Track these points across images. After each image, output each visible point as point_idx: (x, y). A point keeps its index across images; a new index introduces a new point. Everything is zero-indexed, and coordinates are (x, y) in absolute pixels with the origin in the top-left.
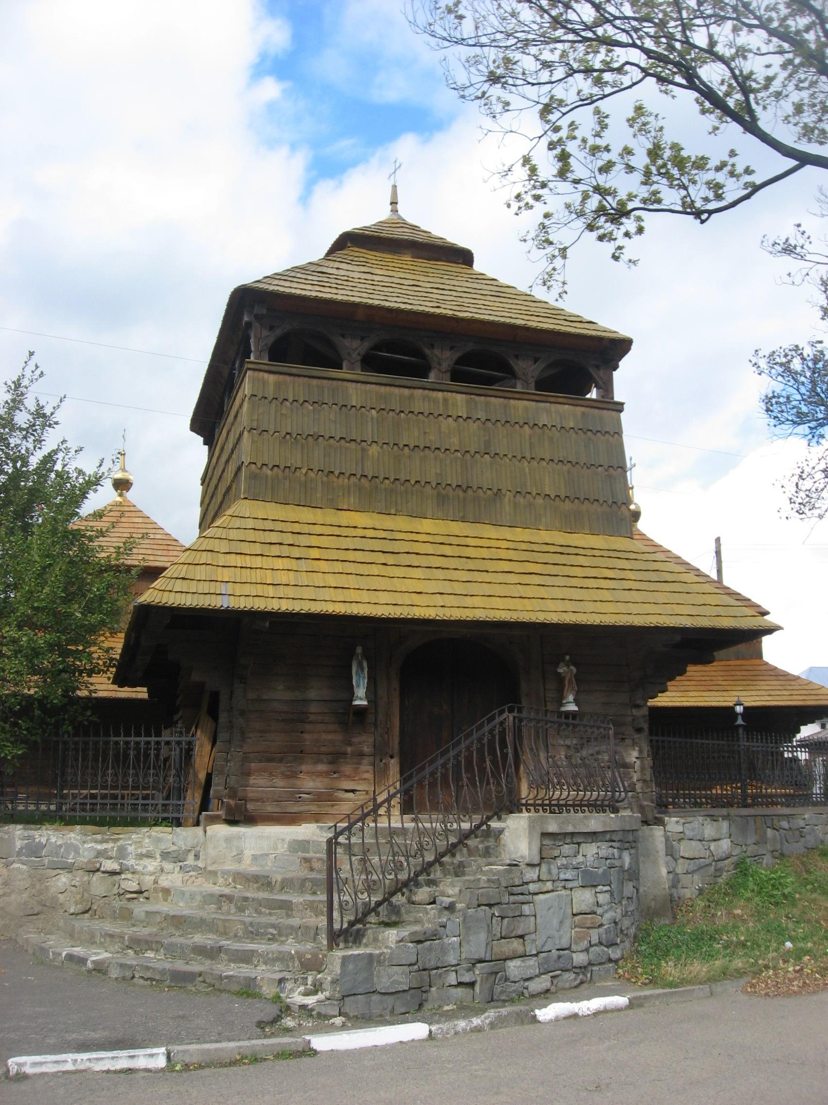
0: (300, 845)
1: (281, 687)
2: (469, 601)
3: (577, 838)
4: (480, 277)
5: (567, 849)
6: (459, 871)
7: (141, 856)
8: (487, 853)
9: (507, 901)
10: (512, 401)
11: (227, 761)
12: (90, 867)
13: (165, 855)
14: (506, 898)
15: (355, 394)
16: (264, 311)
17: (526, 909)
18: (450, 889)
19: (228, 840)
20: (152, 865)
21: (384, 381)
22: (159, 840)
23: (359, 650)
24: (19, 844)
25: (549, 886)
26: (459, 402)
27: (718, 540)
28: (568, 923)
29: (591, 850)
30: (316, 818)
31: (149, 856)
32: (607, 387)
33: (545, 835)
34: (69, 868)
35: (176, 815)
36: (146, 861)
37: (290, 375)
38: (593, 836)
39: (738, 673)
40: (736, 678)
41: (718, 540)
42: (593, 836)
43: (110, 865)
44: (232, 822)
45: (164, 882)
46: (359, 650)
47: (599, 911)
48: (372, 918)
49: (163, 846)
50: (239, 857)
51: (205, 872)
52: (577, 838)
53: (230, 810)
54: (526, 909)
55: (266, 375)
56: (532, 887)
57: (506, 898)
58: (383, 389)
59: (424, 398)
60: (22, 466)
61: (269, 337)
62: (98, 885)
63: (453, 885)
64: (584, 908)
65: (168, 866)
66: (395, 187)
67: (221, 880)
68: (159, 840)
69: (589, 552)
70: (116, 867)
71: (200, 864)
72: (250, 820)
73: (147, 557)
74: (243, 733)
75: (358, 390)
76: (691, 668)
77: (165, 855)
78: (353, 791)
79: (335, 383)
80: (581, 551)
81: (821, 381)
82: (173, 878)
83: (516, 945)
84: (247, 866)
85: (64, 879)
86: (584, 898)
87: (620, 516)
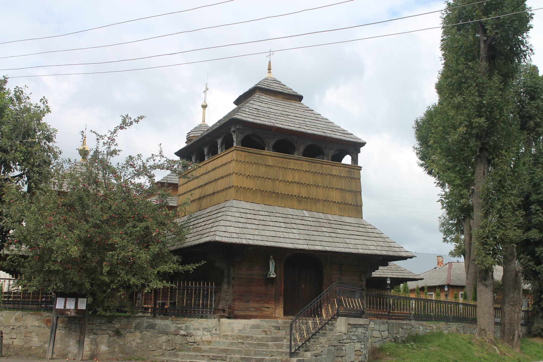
1: (245, 269)
2: (273, 234)
4: (344, 132)
5: (354, 329)
6: (324, 334)
7: (195, 329)
8: (331, 330)
10: (324, 166)
11: (226, 295)
12: (175, 333)
13: (204, 329)
14: (338, 344)
15: (270, 161)
16: (241, 128)
17: (344, 348)
18: (323, 340)
19: (229, 324)
20: (200, 333)
21: (281, 156)
22: (202, 324)
23: (271, 257)
24: (146, 324)
25: (349, 341)
26: (306, 165)
28: (354, 353)
29: (360, 330)
30: (255, 317)
31: (198, 329)
32: (355, 160)
33: (349, 324)
34: (167, 334)
35: (472, 303)
36: (197, 331)
37: (249, 152)
39: (339, 231)
43: (182, 332)
44: (229, 318)
45: (204, 338)
46: (271, 257)
47: (362, 350)
48: (301, 349)
49: (203, 326)
53: (229, 313)
54: (344, 348)
55: (241, 152)
56: (345, 341)
57: (338, 344)
58: (280, 159)
59: (294, 163)
61: (241, 136)
63: (323, 339)
64: (358, 349)
65: (206, 333)
66: (270, 62)
67: (230, 338)
68: (202, 324)
69: (362, 226)
70: (185, 333)
71: (218, 332)
72: (236, 317)
73: (359, 246)
74: (233, 286)
75: (270, 157)
76: (380, 268)
77: (204, 329)
78: (268, 308)
79: (264, 156)
80: (352, 225)
84: (236, 333)
86: (358, 346)
87: (357, 209)
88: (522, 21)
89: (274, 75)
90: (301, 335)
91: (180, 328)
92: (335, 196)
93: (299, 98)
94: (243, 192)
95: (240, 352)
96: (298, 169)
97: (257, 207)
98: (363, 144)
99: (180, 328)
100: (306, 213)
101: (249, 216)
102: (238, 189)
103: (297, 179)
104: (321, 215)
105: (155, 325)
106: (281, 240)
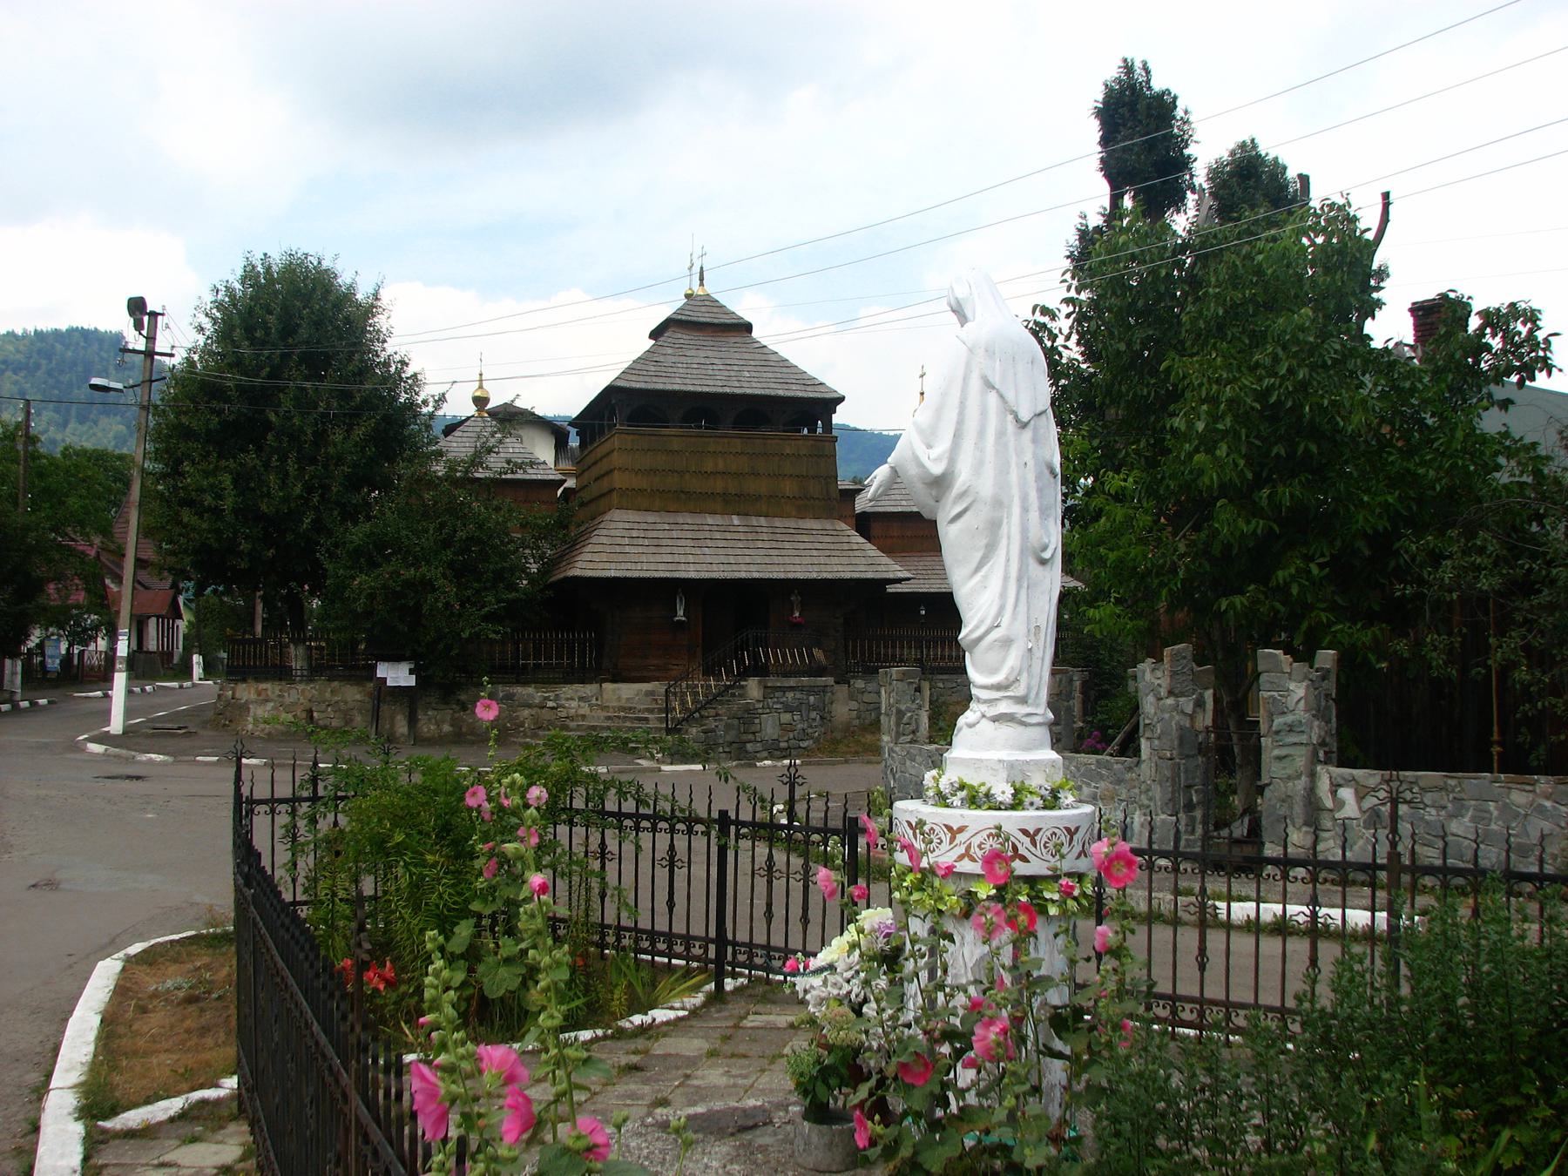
0: (650, 693)
3: (784, 689)
8: (741, 696)
9: (747, 717)
13: (581, 699)
18: (722, 710)
20: (574, 704)
27: (1386, 196)
29: (790, 695)
34: (530, 706)
38: (791, 688)
39: (787, 545)
40: (783, 552)
41: (1386, 196)
42: (791, 688)
43: (550, 704)
44: (614, 681)
45: (581, 712)
50: (619, 699)
51: (604, 708)
52: (784, 689)
60: (1180, 271)
62: (546, 715)
75: (674, 436)
77: (581, 699)
81: (1253, 1097)
82: (585, 710)
83: (751, 737)
85: (526, 712)
86: (786, 717)
88: (11, 335)
89: (710, 288)
90: (683, 703)
91: (547, 698)
92: (789, 487)
93: (748, 328)
94: (636, 499)
95: (609, 728)
96: (725, 451)
97: (651, 517)
98: (842, 399)
99: (547, 698)
100: (736, 520)
101: (635, 534)
102: (623, 492)
103: (721, 466)
104: (763, 521)
105: (513, 695)
106: (792, 568)
